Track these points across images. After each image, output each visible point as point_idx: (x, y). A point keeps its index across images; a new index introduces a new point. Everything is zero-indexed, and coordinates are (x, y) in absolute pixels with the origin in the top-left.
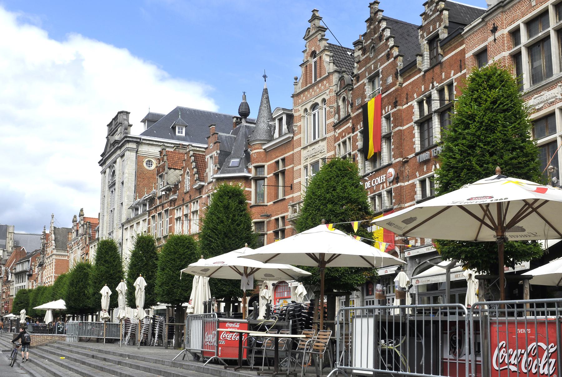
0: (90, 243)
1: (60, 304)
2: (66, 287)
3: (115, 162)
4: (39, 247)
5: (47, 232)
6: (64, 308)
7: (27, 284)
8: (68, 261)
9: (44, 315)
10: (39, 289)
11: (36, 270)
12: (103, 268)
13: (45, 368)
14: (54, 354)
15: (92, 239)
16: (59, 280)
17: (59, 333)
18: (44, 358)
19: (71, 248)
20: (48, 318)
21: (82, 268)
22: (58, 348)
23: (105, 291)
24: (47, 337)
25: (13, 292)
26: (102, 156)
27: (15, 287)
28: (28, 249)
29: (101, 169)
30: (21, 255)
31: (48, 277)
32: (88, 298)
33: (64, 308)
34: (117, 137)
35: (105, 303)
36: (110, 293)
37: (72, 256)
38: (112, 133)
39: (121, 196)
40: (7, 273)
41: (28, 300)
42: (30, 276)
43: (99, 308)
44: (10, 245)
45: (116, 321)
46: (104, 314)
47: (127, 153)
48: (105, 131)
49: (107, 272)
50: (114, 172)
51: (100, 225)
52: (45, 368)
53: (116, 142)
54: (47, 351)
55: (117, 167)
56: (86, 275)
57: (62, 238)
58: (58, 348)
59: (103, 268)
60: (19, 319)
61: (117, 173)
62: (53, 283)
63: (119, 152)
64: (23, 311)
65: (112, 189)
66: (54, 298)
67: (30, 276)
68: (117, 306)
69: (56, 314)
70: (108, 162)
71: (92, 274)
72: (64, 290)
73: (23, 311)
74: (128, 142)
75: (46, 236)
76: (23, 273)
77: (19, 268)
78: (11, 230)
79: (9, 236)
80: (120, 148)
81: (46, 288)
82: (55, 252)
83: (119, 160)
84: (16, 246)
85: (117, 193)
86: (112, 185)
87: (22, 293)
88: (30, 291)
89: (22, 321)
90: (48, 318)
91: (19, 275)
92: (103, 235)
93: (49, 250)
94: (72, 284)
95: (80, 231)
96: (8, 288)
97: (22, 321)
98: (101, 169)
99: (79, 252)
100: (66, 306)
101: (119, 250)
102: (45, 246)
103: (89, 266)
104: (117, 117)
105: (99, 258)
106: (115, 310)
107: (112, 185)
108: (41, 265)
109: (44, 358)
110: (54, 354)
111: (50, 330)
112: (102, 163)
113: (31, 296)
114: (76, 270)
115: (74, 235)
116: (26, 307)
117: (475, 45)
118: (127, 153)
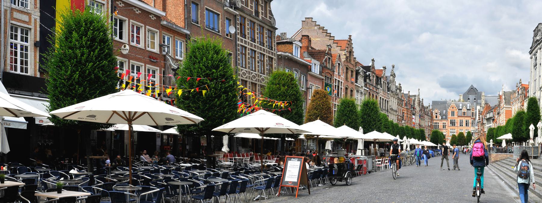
1: (509, 136)
2: (512, 126)
3: (537, 52)
4: (497, 103)
5: (501, 94)
6: (511, 138)
7: (492, 125)
8: (511, 111)
9: (501, 143)
10: (498, 127)
11: (496, 117)
12: (530, 114)
13: (505, 173)
14: (508, 165)
15: (525, 97)
16: (508, 122)
17: (509, 153)
18: (504, 167)
20: (504, 144)
21: (520, 114)
22: (510, 161)
23: (532, 127)
24: (503, 155)
25: (486, 130)
26: (531, 48)
27: (487, 126)
28: (492, 105)
29: (530, 56)
30: (489, 109)
31: (502, 121)
32: (523, 132)
33: (511, 138)
34: (538, 38)
35: (532, 134)
36: (534, 128)
37: (513, 108)
38: (535, 35)
40: (482, 119)
41: (493, 134)
42: (493, 120)
43: (529, 138)
44: (483, 103)
45: (537, 145)
46: (531, 141)
48: (532, 34)
49: (533, 116)
50: (536, 58)
51: (530, 89)
52: (505, 173)
53: (537, 41)
54: (505, 163)
55: (538, 54)
56: (522, 119)
57: (508, 98)
58: (510, 161)
59: (530, 114)
60: (490, 145)
61: (538, 58)
62: (504, 124)
63: (539, 46)
64: (491, 140)
66: (506, 133)
67: (493, 120)
68: (537, 136)
69: (508, 142)
70: (533, 52)
71: (525, 117)
72: (511, 128)
73: (491, 140)
75: (500, 97)
76: (490, 118)
77: (488, 116)
78: (483, 94)
79: (482, 98)
80: (539, 44)
81: (501, 127)
82: (505, 106)
83: (539, 51)
84: (486, 104)
85: (537, 70)
86: (536, 65)
87: (491, 130)
88: (494, 129)
89: (491, 146)
90: (504, 144)
91: (488, 120)
92: (531, 95)
93: (502, 105)
94: (515, 124)
95: (520, 92)
96: (484, 127)
97: (491, 146)
98: (530, 56)
99: (519, 104)
100: (513, 137)
101: (539, 103)
102: (500, 102)
103: (524, 113)
104: (538, 26)
105: (529, 108)
106: (536, 138)
107: (536, 65)
108: (498, 114)
109: (504, 167)
110: (508, 165)
111: (505, 151)
112: (531, 53)
113: (495, 131)
114: (516, 116)
115: (517, 94)
116: (492, 138)
117: (30, 49)
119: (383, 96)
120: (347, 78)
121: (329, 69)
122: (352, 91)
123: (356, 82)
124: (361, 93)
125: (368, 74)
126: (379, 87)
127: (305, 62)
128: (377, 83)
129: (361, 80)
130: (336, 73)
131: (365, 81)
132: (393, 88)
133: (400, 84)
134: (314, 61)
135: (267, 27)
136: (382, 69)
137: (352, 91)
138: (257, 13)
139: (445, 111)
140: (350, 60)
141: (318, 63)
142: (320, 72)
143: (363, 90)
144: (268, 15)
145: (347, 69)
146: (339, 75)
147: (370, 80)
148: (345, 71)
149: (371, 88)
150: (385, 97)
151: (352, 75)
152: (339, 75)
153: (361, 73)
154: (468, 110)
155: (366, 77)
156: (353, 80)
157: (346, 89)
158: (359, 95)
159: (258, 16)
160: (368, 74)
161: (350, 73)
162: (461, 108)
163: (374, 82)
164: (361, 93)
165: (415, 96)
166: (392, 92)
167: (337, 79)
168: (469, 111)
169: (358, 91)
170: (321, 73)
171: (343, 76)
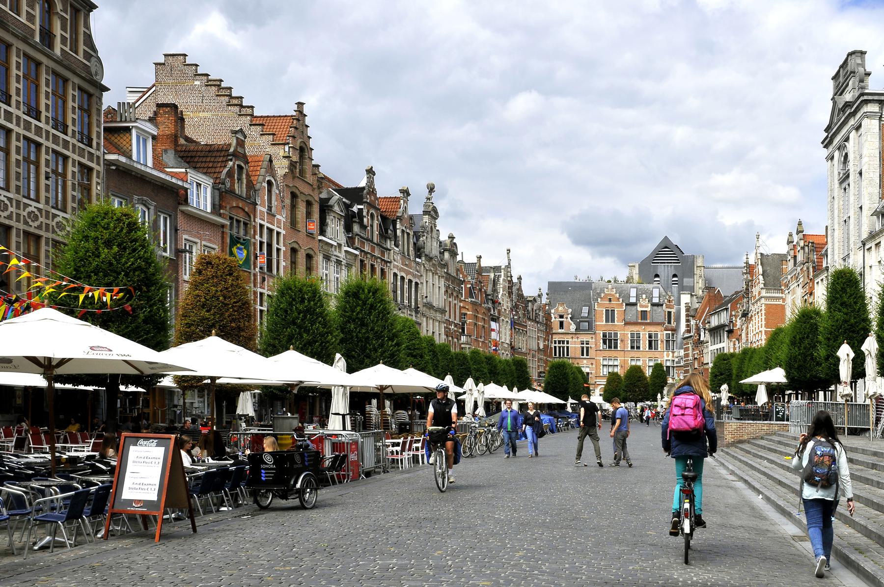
0: (815, 276)
19: (787, 286)
39: (859, 196)
47: (866, 122)
53: (848, 105)
63: (852, 122)
65: (845, 185)
67: (730, 332)
74: (867, 102)
76: (720, 327)
80: (853, 114)
82: (764, 293)
83: (853, 135)
96: (701, 353)
118: (866, 122)
119: (401, 270)
120: (293, 223)
121: (239, 197)
122: (309, 257)
123: (322, 232)
124: (339, 262)
125: (355, 209)
126: (389, 244)
127: (168, 178)
128: (384, 236)
129: (336, 230)
130: (261, 209)
131: (348, 228)
132: (432, 248)
133: (452, 238)
134: (194, 176)
135: (77, 80)
136: (399, 195)
137: (309, 257)
138: (47, 36)
139: (585, 310)
140: (302, 172)
141: (207, 182)
142: (213, 205)
143: (342, 255)
144: (82, 47)
145: (294, 196)
146: (271, 215)
147: (363, 227)
148: (288, 201)
149: (367, 249)
150: (408, 273)
151: (309, 214)
152: (271, 215)
153: (336, 208)
154: (653, 305)
155: (350, 220)
156: (314, 227)
157: (294, 251)
158: (332, 267)
159: (51, 46)
160: (355, 209)
161: (302, 209)
162: (633, 300)
163: (376, 233)
164: (339, 262)
165: (497, 269)
166: (430, 259)
167: (266, 224)
168: (659, 309)
169: (327, 258)
170: (216, 208)
171: (282, 217)
